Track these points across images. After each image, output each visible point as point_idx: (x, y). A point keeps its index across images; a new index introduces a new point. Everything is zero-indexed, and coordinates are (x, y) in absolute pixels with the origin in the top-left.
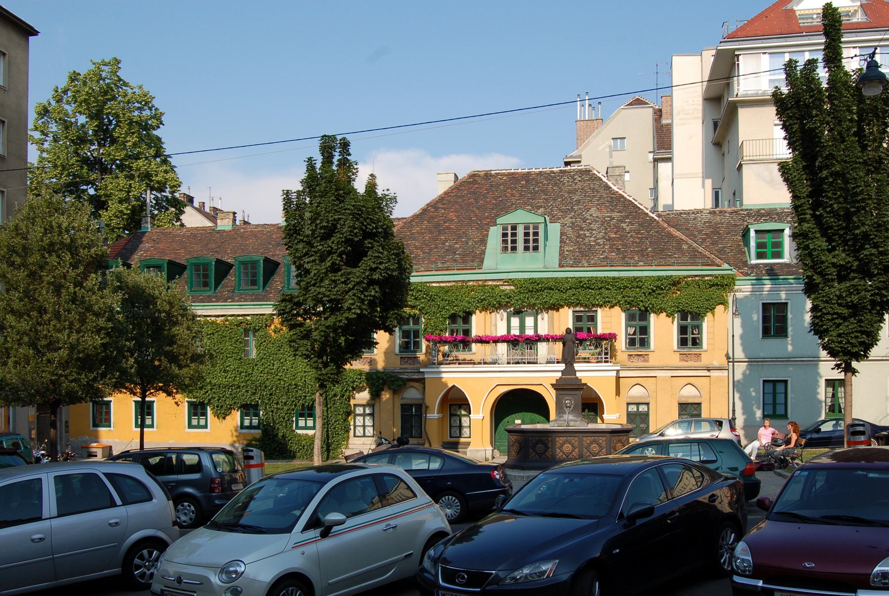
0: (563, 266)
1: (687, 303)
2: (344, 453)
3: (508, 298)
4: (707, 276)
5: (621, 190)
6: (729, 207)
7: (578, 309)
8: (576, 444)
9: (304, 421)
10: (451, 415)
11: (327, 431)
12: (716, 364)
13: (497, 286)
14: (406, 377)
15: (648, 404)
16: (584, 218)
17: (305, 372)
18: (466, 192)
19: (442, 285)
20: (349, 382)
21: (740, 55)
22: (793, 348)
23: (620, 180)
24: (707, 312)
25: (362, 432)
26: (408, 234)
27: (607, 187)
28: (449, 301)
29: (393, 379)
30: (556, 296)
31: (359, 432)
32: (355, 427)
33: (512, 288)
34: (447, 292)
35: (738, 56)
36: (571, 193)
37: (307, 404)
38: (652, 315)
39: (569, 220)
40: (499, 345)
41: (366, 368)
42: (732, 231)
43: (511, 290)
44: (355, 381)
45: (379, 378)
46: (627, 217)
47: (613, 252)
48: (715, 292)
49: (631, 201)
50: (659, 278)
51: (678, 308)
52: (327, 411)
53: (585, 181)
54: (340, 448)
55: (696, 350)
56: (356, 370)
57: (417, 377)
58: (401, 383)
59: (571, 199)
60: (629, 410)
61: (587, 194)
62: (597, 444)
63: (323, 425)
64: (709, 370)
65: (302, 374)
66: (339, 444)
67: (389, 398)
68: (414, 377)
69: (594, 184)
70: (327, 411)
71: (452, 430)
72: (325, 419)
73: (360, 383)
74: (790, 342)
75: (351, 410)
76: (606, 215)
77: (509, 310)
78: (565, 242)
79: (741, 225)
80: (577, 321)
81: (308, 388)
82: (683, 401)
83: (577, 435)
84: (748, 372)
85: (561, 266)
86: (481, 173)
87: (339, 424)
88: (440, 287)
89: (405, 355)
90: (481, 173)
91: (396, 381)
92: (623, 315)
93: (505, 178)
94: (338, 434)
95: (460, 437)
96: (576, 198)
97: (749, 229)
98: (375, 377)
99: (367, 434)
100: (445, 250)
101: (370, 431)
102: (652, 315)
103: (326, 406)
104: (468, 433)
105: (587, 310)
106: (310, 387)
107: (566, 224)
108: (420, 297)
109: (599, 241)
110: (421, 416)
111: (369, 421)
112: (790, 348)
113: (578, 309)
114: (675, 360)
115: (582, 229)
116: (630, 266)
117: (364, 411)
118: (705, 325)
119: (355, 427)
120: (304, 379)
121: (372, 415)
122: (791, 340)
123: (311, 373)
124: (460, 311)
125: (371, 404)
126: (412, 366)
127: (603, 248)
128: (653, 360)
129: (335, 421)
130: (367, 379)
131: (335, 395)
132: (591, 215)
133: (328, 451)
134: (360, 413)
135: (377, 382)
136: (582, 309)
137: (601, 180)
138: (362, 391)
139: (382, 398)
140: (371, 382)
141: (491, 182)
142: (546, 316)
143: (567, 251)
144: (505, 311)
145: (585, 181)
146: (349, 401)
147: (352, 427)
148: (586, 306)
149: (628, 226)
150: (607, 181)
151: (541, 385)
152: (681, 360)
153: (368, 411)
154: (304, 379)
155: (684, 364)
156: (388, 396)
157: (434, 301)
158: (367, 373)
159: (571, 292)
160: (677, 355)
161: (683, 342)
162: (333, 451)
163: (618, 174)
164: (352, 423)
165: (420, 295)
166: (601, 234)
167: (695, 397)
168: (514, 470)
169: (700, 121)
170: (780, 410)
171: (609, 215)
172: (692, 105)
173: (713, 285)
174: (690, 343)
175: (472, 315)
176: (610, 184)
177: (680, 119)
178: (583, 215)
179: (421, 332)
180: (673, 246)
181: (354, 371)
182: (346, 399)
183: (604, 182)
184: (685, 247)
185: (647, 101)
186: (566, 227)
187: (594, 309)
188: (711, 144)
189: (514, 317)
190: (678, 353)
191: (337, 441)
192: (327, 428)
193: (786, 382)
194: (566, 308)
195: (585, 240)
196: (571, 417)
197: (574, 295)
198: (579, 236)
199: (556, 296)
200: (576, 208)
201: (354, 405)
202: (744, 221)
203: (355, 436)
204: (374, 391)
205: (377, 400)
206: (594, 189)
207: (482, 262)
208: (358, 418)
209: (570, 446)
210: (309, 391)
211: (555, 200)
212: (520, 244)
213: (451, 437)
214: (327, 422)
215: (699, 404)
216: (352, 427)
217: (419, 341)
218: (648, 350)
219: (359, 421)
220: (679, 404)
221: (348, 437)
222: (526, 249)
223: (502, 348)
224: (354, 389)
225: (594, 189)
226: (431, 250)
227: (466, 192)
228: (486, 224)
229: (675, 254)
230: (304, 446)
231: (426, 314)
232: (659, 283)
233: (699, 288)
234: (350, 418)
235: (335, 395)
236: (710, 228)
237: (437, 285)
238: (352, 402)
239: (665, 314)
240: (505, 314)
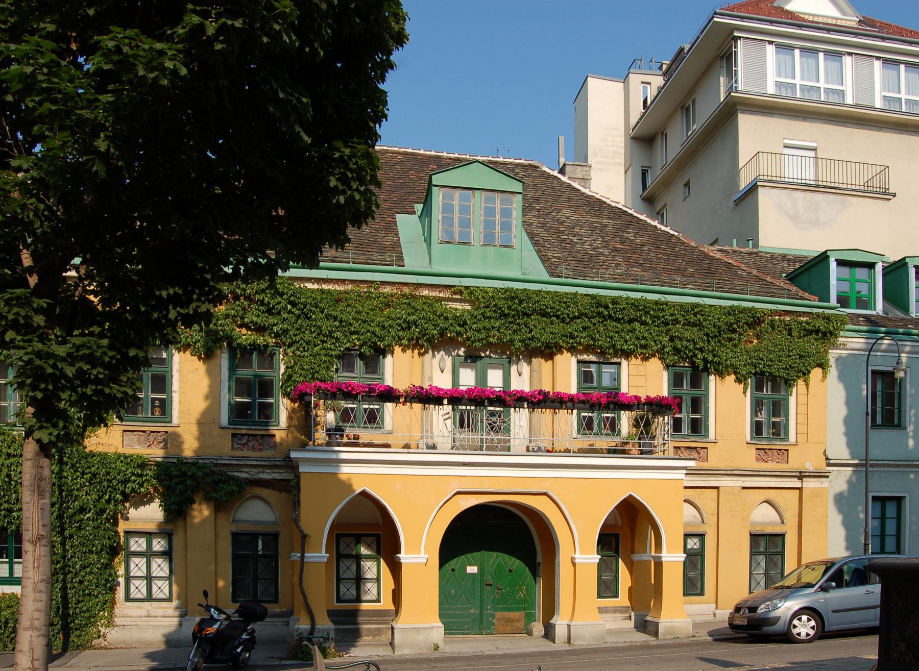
3: (460, 326)
7: (585, 357)
10: (340, 557)
11: (64, 589)
12: (809, 467)
13: (440, 300)
14: (244, 475)
17: (9, 455)
19: (325, 287)
20: (115, 482)
21: (740, 38)
24: (799, 377)
25: (144, 591)
28: (341, 322)
29: (216, 478)
30: (543, 331)
31: (139, 588)
32: (128, 579)
34: (338, 301)
35: (736, 39)
37: (14, 527)
38: (712, 378)
40: (563, 413)
43: (464, 311)
44: (129, 481)
48: (810, 345)
50: (731, 311)
51: (755, 367)
52: (63, 544)
54: (94, 624)
55: (778, 443)
56: (132, 456)
57: (269, 477)
58: (234, 488)
60: (689, 547)
63: (53, 575)
66: (91, 617)
67: (207, 518)
70: (63, 544)
71: (341, 586)
72: (58, 562)
73: (141, 485)
74: (911, 434)
75: (119, 543)
82: (758, 530)
84: (854, 479)
87: (91, 573)
88: (322, 291)
91: (224, 482)
92: (665, 374)
94: (89, 595)
98: (175, 473)
99: (156, 593)
101: (161, 588)
102: (712, 378)
103: (61, 532)
108: (279, 307)
110: (275, 558)
111: (160, 567)
112: (911, 442)
117: (149, 545)
118: (792, 400)
119: (128, 579)
121: (167, 554)
122: (913, 431)
124: (364, 344)
125: (166, 531)
126: (257, 454)
128: (716, 459)
129: (83, 567)
130: (158, 477)
131: (82, 510)
133: (66, 630)
134: (139, 549)
135: (179, 483)
138: (144, 504)
140: (168, 483)
142: (525, 367)
144: (448, 353)
147: (121, 580)
151: (545, 494)
153: (159, 545)
155: (762, 466)
156: (206, 512)
157: (309, 319)
158: (158, 464)
159: (579, 324)
162: (78, 633)
164: (121, 571)
165: (279, 303)
167: (772, 524)
169: (622, 170)
172: (613, 146)
173: (810, 332)
174: (686, 428)
175: (384, 357)
181: (126, 457)
182: (107, 520)
187: (615, 360)
189: (465, 367)
190: (754, 447)
191: (88, 611)
192: (64, 581)
194: (566, 355)
197: (585, 328)
199: (543, 331)
201: (127, 533)
203: (128, 598)
204: (174, 503)
205: (180, 524)
208: (135, 561)
213: (339, 600)
214: (63, 568)
215: (782, 536)
216: (121, 580)
218: (705, 440)
219: (138, 566)
220: (751, 535)
221: (113, 602)
222: (489, 241)
223: (569, 420)
224: (126, 497)
231: (290, 346)
232: (731, 319)
233: (790, 334)
234: (117, 560)
235: (82, 510)
237: (316, 286)
238: (122, 526)
240: (448, 361)
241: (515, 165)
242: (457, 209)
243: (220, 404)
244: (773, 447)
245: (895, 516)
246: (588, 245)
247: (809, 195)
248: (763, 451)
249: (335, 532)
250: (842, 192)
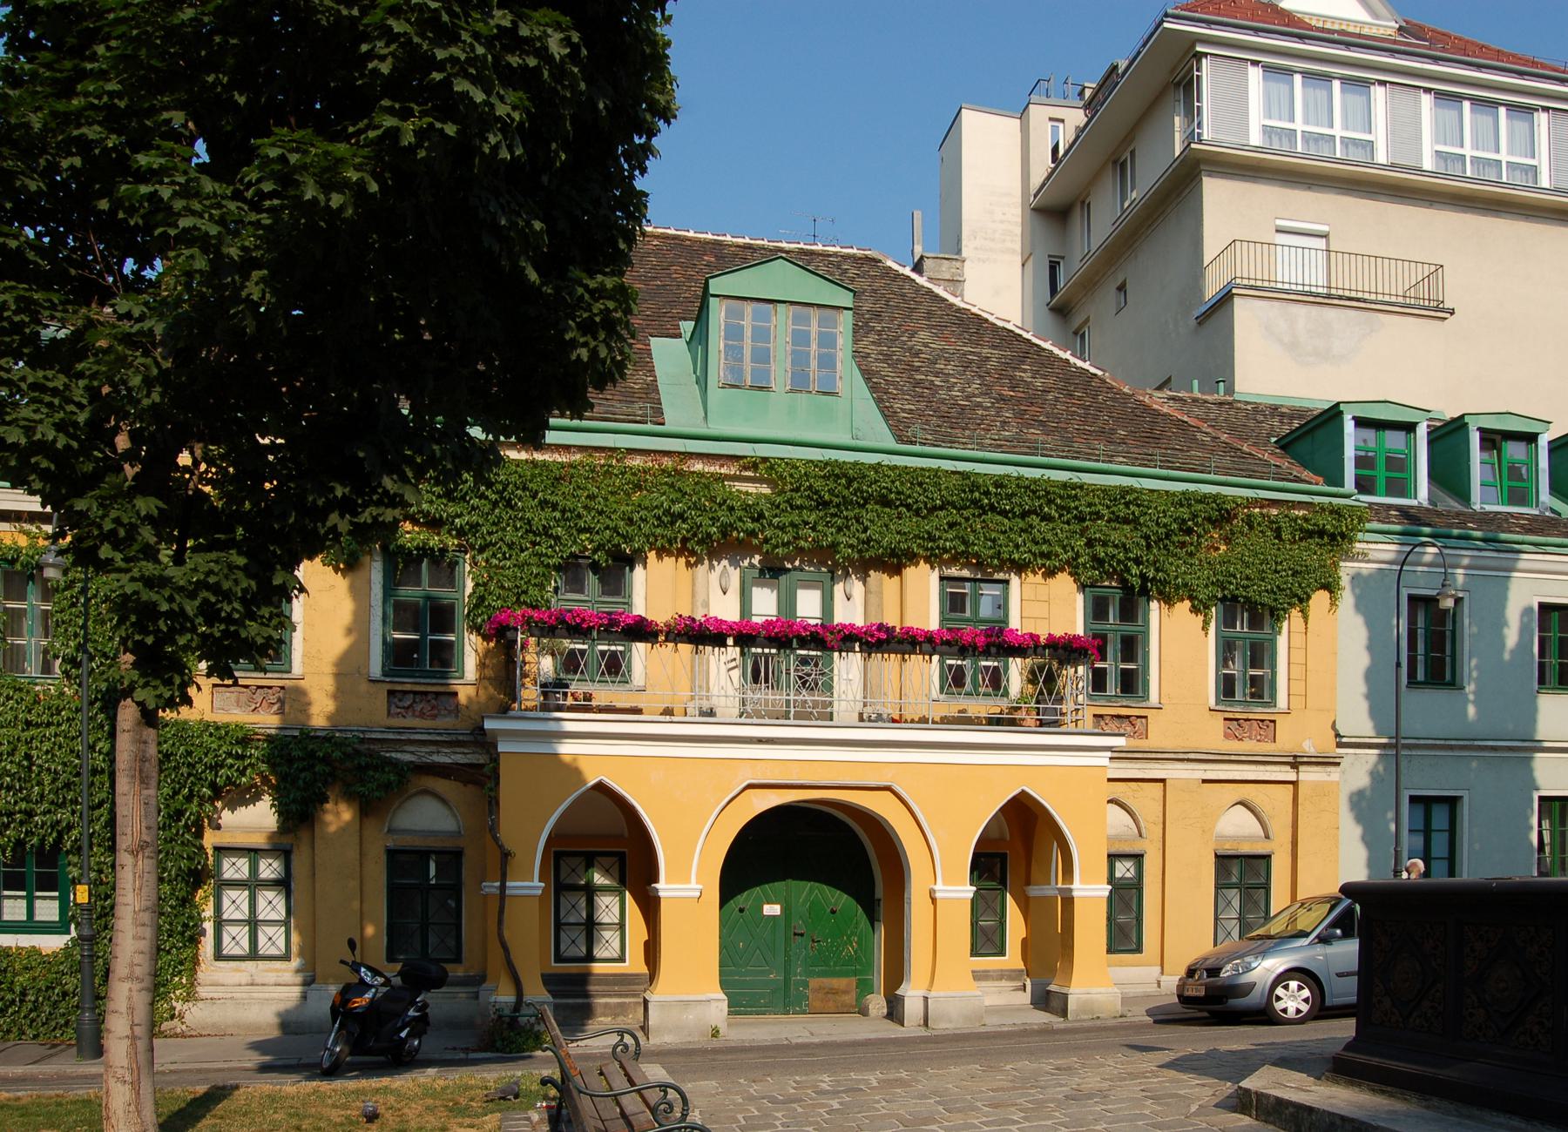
1: (1248, 578)
2: (181, 1017)
4: (1301, 505)
7: (953, 571)
9: (24, 903)
12: (1309, 748)
14: (407, 757)
15: (1138, 858)
17: (28, 724)
21: (1206, 55)
22: (1478, 712)
25: (245, 943)
28: (563, 511)
29: (363, 761)
30: (886, 530)
32: (219, 924)
33: (766, 490)
35: (1199, 56)
37: (35, 840)
38: (1154, 605)
41: (267, 721)
45: (312, 754)
48: (1310, 553)
50: (1185, 499)
51: (1224, 589)
55: (1260, 710)
56: (227, 725)
57: (447, 760)
60: (1118, 875)
64: (1295, 765)
65: (15, 732)
67: (348, 824)
68: (436, 758)
73: (242, 773)
74: (1471, 697)
77: (746, 563)
80: (953, 609)
81: (40, 783)
82: (1228, 848)
89: (408, 684)
91: (376, 768)
95: (590, 958)
97: (1342, 412)
101: (272, 939)
102: (1154, 605)
104: (616, 944)
105: (979, 576)
106: (47, 779)
111: (272, 905)
112: (1471, 710)
113: (953, 571)
114: (1212, 734)
116: (1098, 461)
117: (254, 869)
118: (1282, 642)
119: (219, 924)
120: (23, 749)
121: (283, 884)
123: (52, 729)
125: (280, 847)
126: (429, 723)
130: (268, 759)
134: (237, 876)
135: (303, 770)
136: (966, 573)
138: (246, 803)
139: (327, 824)
146: (199, 834)
147: (209, 926)
148: (980, 565)
151: (888, 789)
152: (1226, 736)
153: (269, 869)
154: (23, 749)
155: (1233, 746)
158: (270, 739)
159: (943, 517)
160: (1218, 723)
161: (1227, 687)
164: (208, 912)
167: (1250, 839)
177: (976, 248)
179: (462, 611)
181: (218, 728)
187: (1001, 576)
188: (1046, 308)
189: (762, 586)
190: (1221, 716)
193: (1452, 802)
194: (923, 567)
197: (951, 525)
203: (219, 956)
205: (304, 835)
208: (230, 895)
210: (42, 796)
213: (559, 958)
215: (1267, 858)
216: (209, 926)
217: (452, 643)
218: (1144, 704)
219: (235, 903)
220: (1217, 856)
221: (195, 961)
222: (799, 385)
224: (217, 792)
230: (24, 994)
232: (1184, 512)
238: (210, 839)
239: (1187, 603)
240: (735, 576)
242: (748, 333)
244: (1251, 716)
246: (959, 391)
247: (1315, 310)
248: (1235, 723)
250: (1368, 306)
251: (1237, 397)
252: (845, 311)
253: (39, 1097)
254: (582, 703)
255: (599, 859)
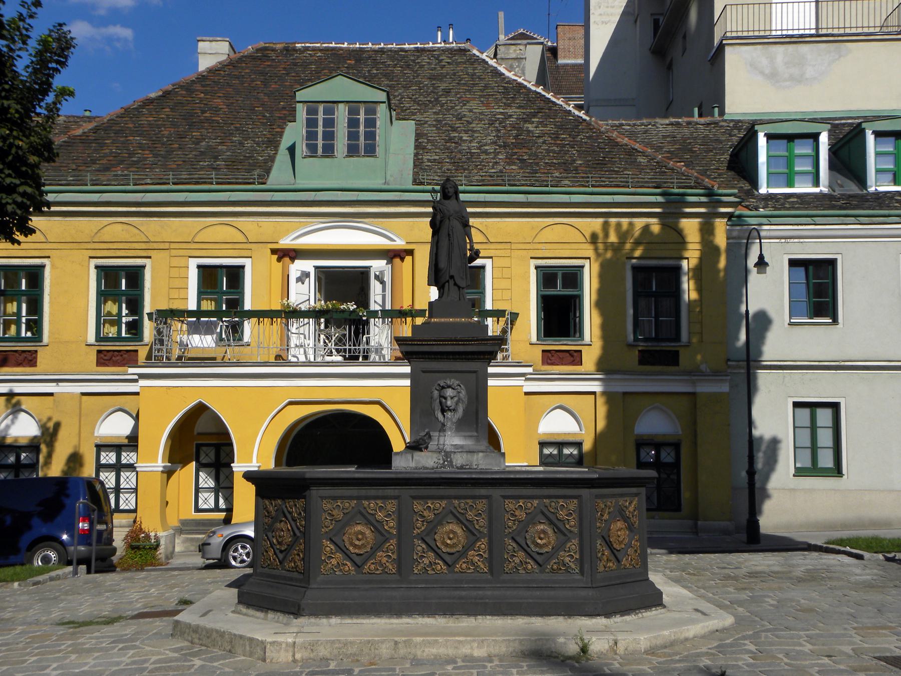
0: (422, 184)
5: (520, 77)
6: (700, 115)
8: (481, 523)
16: (459, 114)
18: (247, 71)
23: (518, 66)
26: (131, 126)
27: (496, 73)
36: (434, 79)
39: (432, 116)
42: (715, 149)
46: (534, 115)
47: (514, 164)
49: (539, 93)
53: (458, 64)
59: (435, 88)
61: (462, 82)
62: (551, 523)
69: (475, 69)
76: (498, 110)
78: (424, 148)
79: (729, 141)
82: (98, 442)
83: (483, 491)
85: (416, 182)
86: (278, 46)
90: (278, 46)
93: (319, 54)
96: (443, 86)
100: (197, 153)
107: (426, 122)
109: (487, 148)
115: (454, 130)
127: (493, 158)
132: (471, 111)
137: (487, 63)
141: (293, 59)
143: (429, 160)
145: (458, 64)
149: (536, 127)
150: (495, 65)
151: (378, 403)
163: (514, 56)
166: (490, 138)
168: (271, 615)
170: (826, 460)
171: (501, 110)
176: (502, 69)
177: (601, 15)
178: (456, 110)
180: (620, 158)
183: (492, 66)
184: (642, 160)
185: (535, 36)
186: (426, 125)
193: (835, 407)
195: (460, 145)
196: (457, 441)
198: (451, 140)
200: (443, 100)
202: (731, 135)
206: (474, 74)
207: (268, 171)
209: (458, 530)
211: (406, 88)
212: (341, 142)
213: (198, 510)
222: (353, 151)
225: (474, 74)
226: (170, 152)
227: (247, 71)
228: (280, 118)
229: (626, 169)
236: (675, 144)
241: (443, 50)
242: (320, 123)
243: (87, 323)
245: (808, 425)
246: (476, 143)
247: (791, 48)
249: (195, 442)
250: (836, 38)
251: (726, 117)
252: (381, 104)
253: (312, 646)
254: (153, 354)
255: (641, 458)
